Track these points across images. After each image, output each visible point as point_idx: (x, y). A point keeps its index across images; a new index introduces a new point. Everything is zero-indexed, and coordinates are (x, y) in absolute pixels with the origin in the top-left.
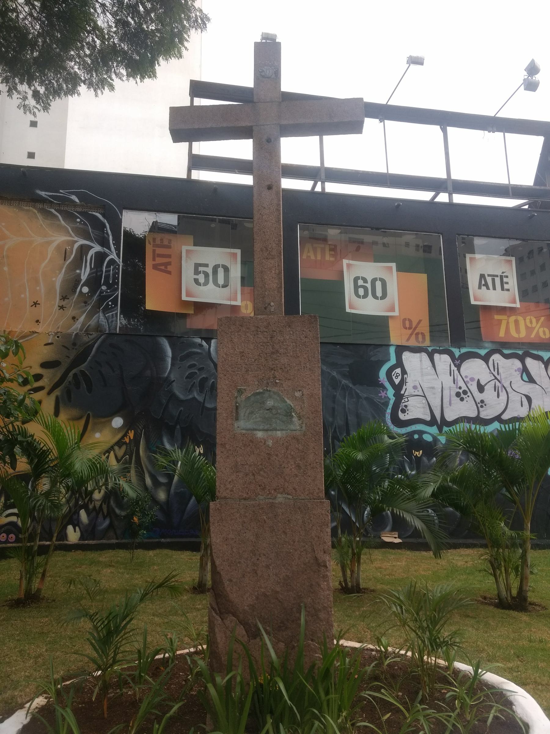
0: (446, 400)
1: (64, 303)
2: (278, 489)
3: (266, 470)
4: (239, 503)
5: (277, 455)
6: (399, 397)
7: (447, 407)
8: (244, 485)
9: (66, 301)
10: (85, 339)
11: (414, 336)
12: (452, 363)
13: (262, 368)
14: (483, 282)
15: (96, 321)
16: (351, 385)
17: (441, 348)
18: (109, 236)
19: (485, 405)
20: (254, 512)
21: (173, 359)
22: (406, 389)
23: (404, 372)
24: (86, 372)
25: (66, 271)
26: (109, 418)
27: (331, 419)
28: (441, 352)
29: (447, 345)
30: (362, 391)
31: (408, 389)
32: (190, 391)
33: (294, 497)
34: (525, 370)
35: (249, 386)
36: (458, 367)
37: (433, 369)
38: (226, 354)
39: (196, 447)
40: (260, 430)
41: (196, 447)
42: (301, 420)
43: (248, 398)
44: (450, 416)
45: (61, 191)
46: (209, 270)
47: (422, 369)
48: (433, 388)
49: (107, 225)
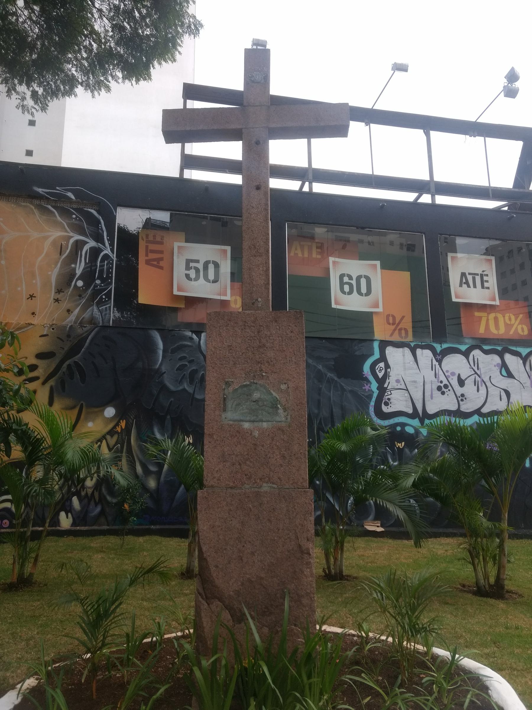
0: (428, 394)
1: (58, 296)
2: (264, 478)
3: (252, 460)
4: (226, 492)
5: (263, 446)
6: (382, 390)
7: (429, 400)
8: (230, 474)
9: (62, 294)
10: (80, 331)
11: (397, 332)
12: (433, 358)
13: (249, 361)
14: (464, 281)
15: (90, 313)
16: (336, 378)
17: (423, 344)
18: (103, 232)
19: (466, 399)
20: (240, 500)
21: (164, 351)
22: (389, 383)
23: (387, 366)
24: (80, 363)
25: (61, 265)
26: (102, 408)
27: (316, 411)
28: (423, 347)
29: (429, 341)
30: (347, 384)
31: (391, 383)
32: (181, 382)
33: (279, 487)
34: (504, 365)
35: (236, 378)
36: (440, 362)
37: (415, 363)
38: (214, 348)
39: (186, 437)
40: (246, 421)
41: (186, 437)
42: (286, 412)
43: (235, 390)
44: (431, 409)
45: (57, 188)
46: (200, 266)
47: (404, 363)
48: (415, 382)
49: (102, 221)
